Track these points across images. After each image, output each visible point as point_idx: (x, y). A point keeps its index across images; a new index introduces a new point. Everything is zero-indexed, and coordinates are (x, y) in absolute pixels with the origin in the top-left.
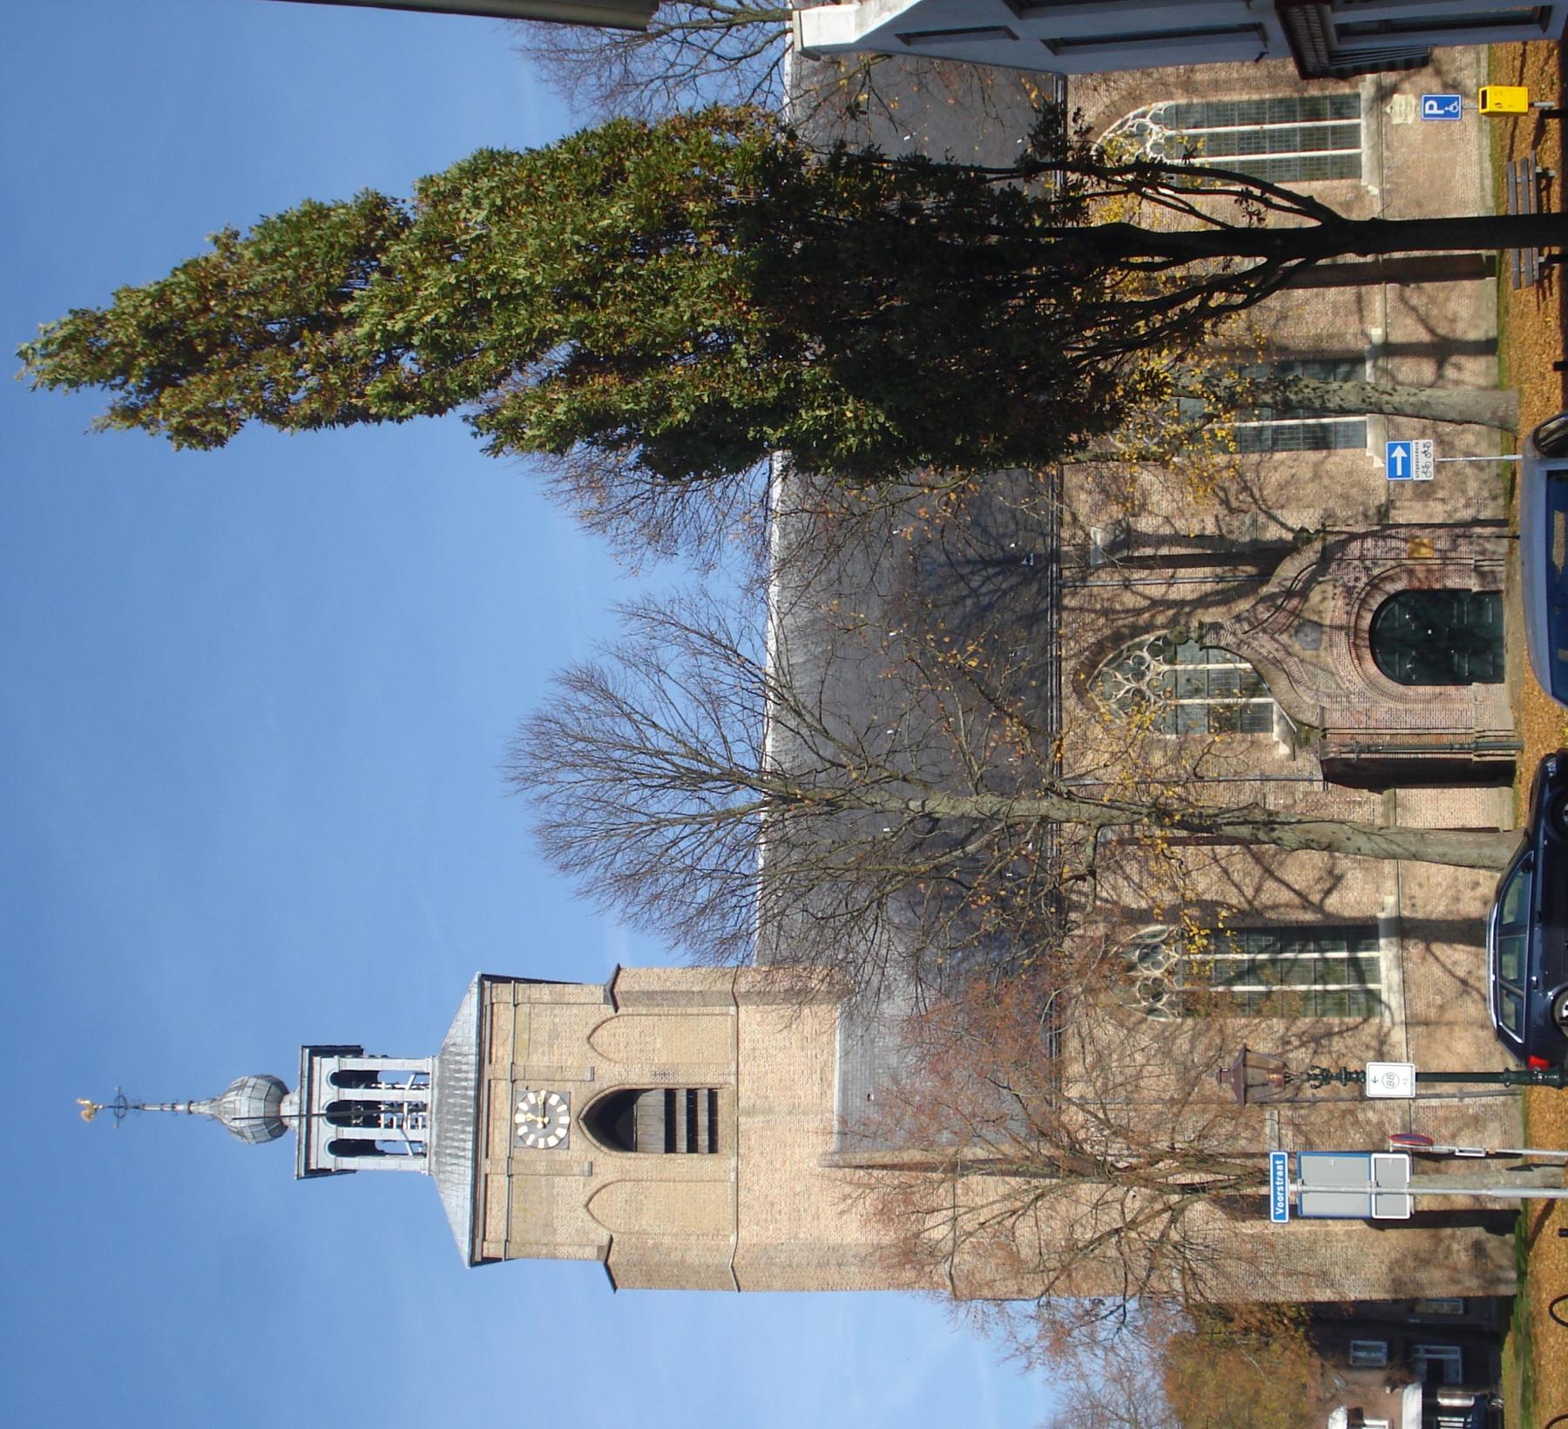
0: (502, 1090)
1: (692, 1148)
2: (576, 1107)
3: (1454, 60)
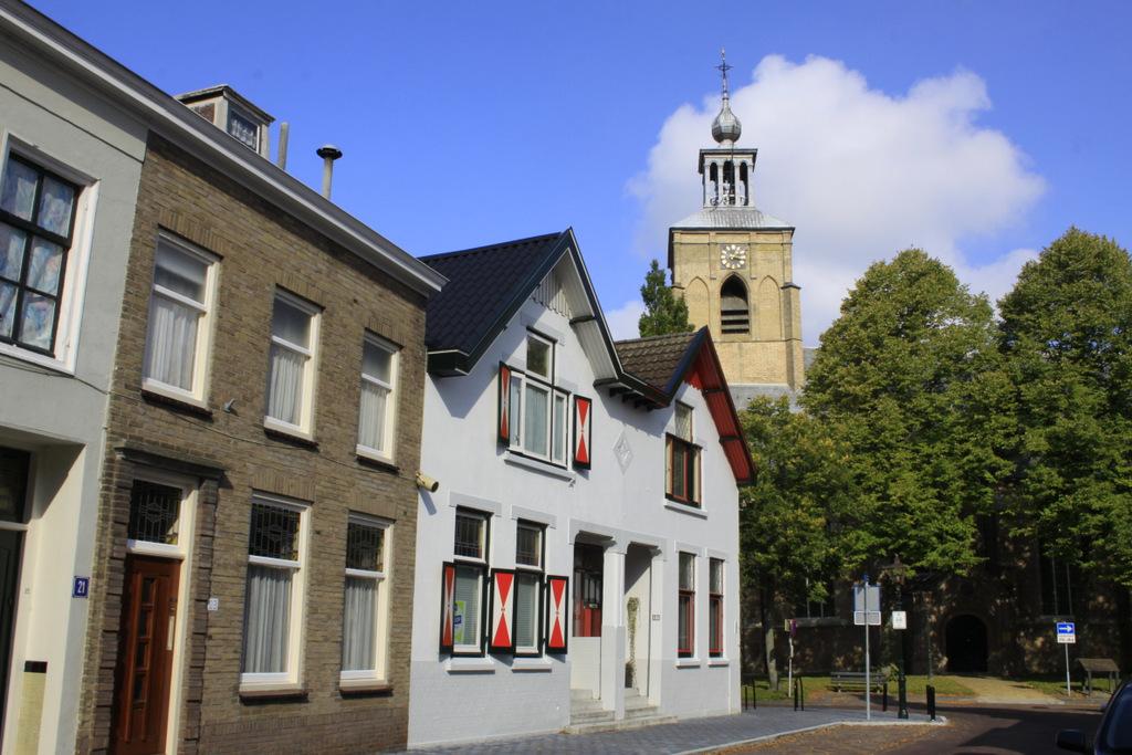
0: (745, 239)
1: (724, 323)
2: (740, 272)
3: (1086, 519)
